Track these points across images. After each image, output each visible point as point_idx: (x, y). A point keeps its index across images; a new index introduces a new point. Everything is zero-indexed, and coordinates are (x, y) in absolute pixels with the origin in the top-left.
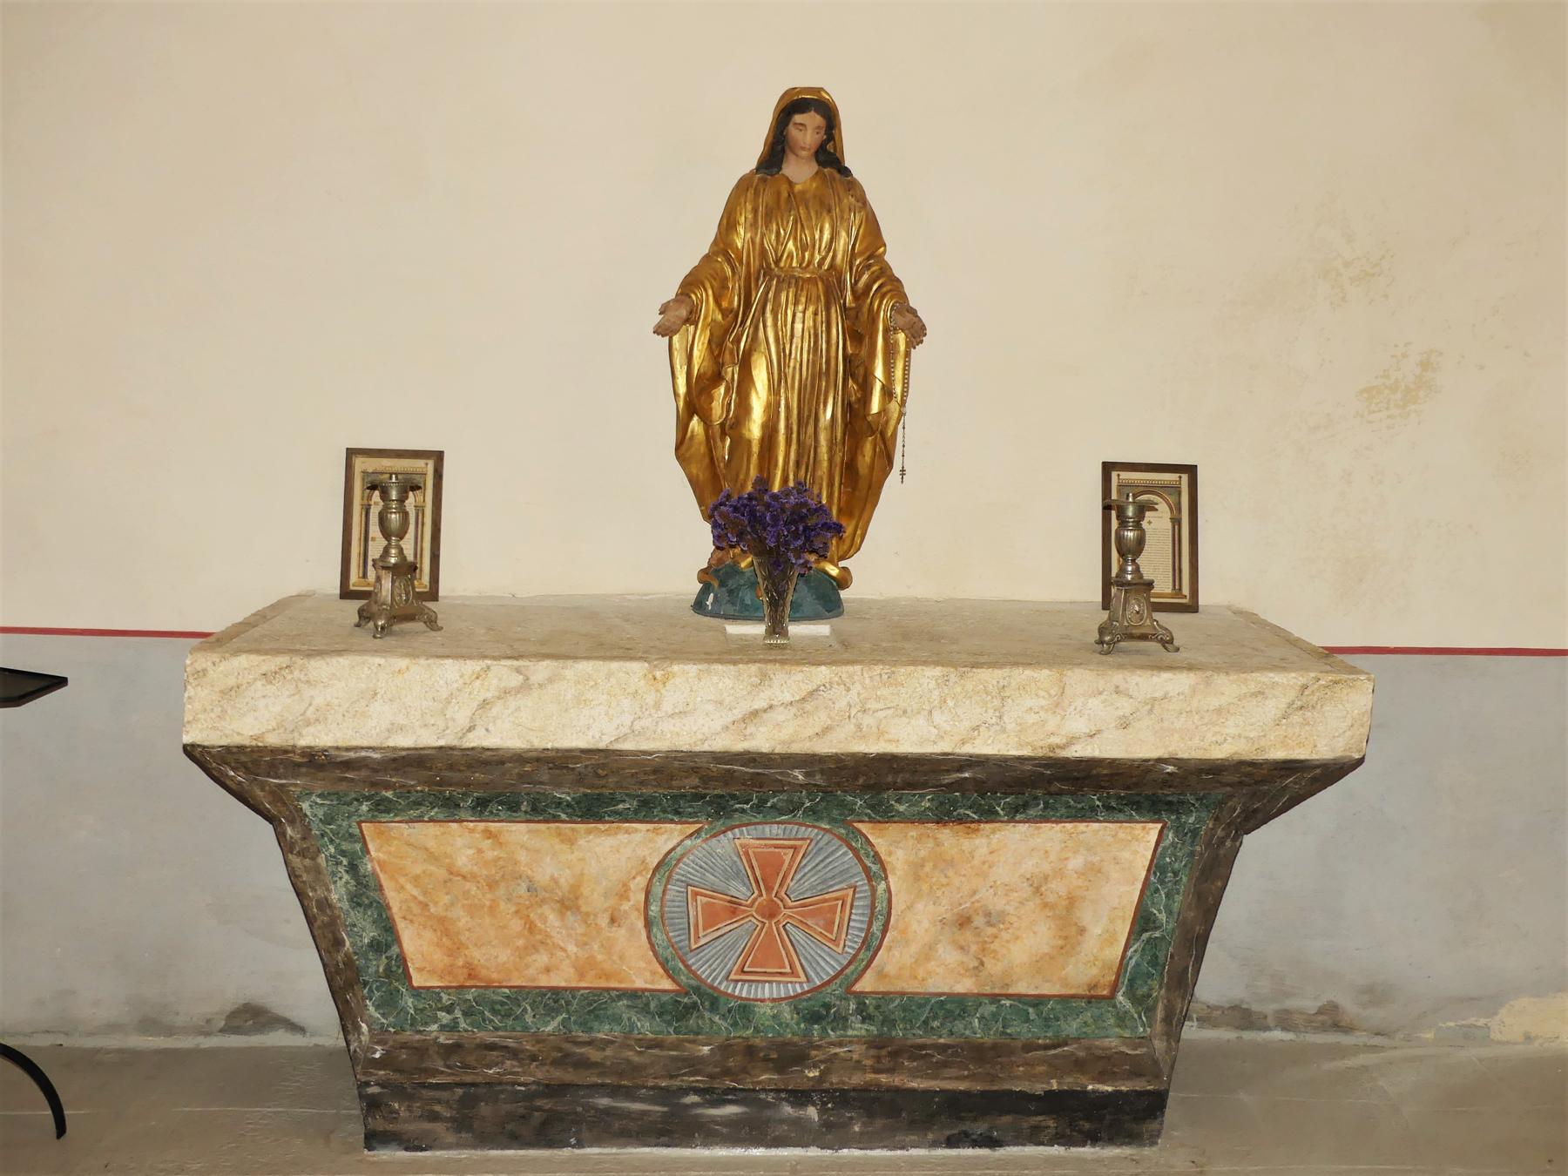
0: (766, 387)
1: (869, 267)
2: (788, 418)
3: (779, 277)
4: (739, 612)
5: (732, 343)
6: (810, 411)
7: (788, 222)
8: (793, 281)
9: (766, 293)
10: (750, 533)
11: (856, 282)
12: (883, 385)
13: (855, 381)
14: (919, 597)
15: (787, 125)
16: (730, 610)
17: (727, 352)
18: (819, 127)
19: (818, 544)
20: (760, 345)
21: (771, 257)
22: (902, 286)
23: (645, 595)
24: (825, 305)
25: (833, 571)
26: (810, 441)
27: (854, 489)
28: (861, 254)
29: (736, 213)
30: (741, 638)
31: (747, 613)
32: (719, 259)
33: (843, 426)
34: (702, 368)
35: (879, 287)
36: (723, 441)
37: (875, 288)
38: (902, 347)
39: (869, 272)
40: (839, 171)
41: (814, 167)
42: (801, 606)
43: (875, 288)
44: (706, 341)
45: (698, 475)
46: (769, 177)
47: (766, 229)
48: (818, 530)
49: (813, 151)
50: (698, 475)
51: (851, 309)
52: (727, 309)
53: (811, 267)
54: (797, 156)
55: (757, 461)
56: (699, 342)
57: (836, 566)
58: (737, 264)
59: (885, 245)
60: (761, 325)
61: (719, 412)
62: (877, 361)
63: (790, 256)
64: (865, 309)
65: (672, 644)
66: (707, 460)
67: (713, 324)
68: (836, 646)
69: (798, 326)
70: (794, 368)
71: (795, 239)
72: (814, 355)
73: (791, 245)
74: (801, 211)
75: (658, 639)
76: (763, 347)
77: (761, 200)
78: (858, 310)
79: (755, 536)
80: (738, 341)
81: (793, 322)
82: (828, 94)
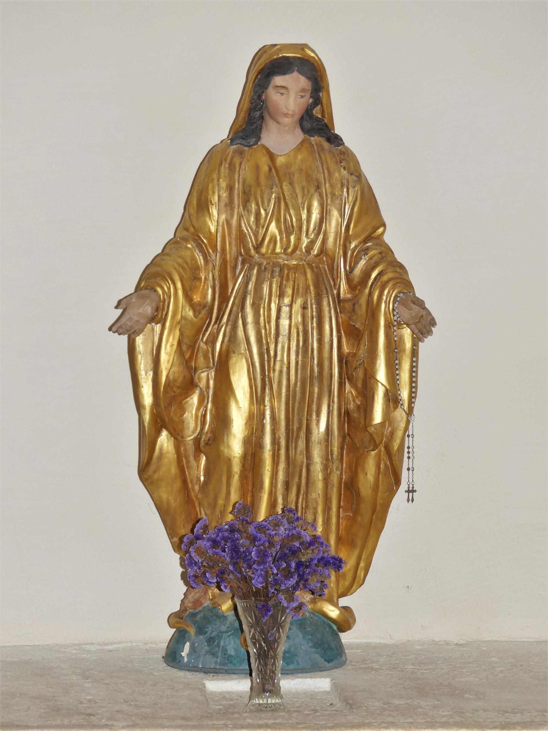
0: (248, 395)
1: (366, 251)
2: (274, 432)
3: (260, 265)
4: (220, 664)
5: (206, 343)
6: (300, 422)
7: (269, 201)
8: (277, 269)
9: (246, 283)
10: (233, 573)
11: (352, 269)
12: (387, 391)
13: (353, 385)
14: (437, 640)
15: (266, 88)
16: (211, 662)
17: (200, 355)
18: (303, 90)
19: (313, 582)
20: (239, 345)
21: (251, 241)
22: (406, 272)
23: (107, 644)
24: (315, 296)
25: (333, 612)
26: (301, 458)
27: (356, 512)
28: (356, 236)
29: (208, 194)
30: (224, 696)
31: (230, 666)
32: (189, 246)
33: (340, 439)
34: (171, 373)
35: (380, 274)
36: (197, 459)
37: (374, 275)
38: (408, 345)
39: (367, 257)
40: (329, 140)
41: (299, 136)
42: (296, 655)
43: (374, 275)
44: (175, 343)
45: (168, 500)
46: (246, 148)
47: (244, 209)
48: (313, 566)
49: (297, 117)
50: (168, 500)
51: (346, 300)
52: (199, 304)
53: (298, 252)
54: (278, 122)
55: (238, 483)
56: (166, 345)
57: (336, 605)
58: (211, 251)
59: (384, 225)
60: (240, 322)
61: (192, 425)
62: (378, 362)
63: (273, 240)
64: (363, 300)
65: (143, 707)
66: (178, 484)
67: (183, 322)
68: (339, 705)
69: (285, 323)
70: (281, 372)
71: (278, 221)
72: (303, 357)
73: (273, 227)
74: (285, 188)
75: (126, 702)
76: (243, 347)
77: (236, 177)
78: (354, 301)
79: (239, 575)
80: (212, 341)
81: (278, 318)
82: (313, 51)
